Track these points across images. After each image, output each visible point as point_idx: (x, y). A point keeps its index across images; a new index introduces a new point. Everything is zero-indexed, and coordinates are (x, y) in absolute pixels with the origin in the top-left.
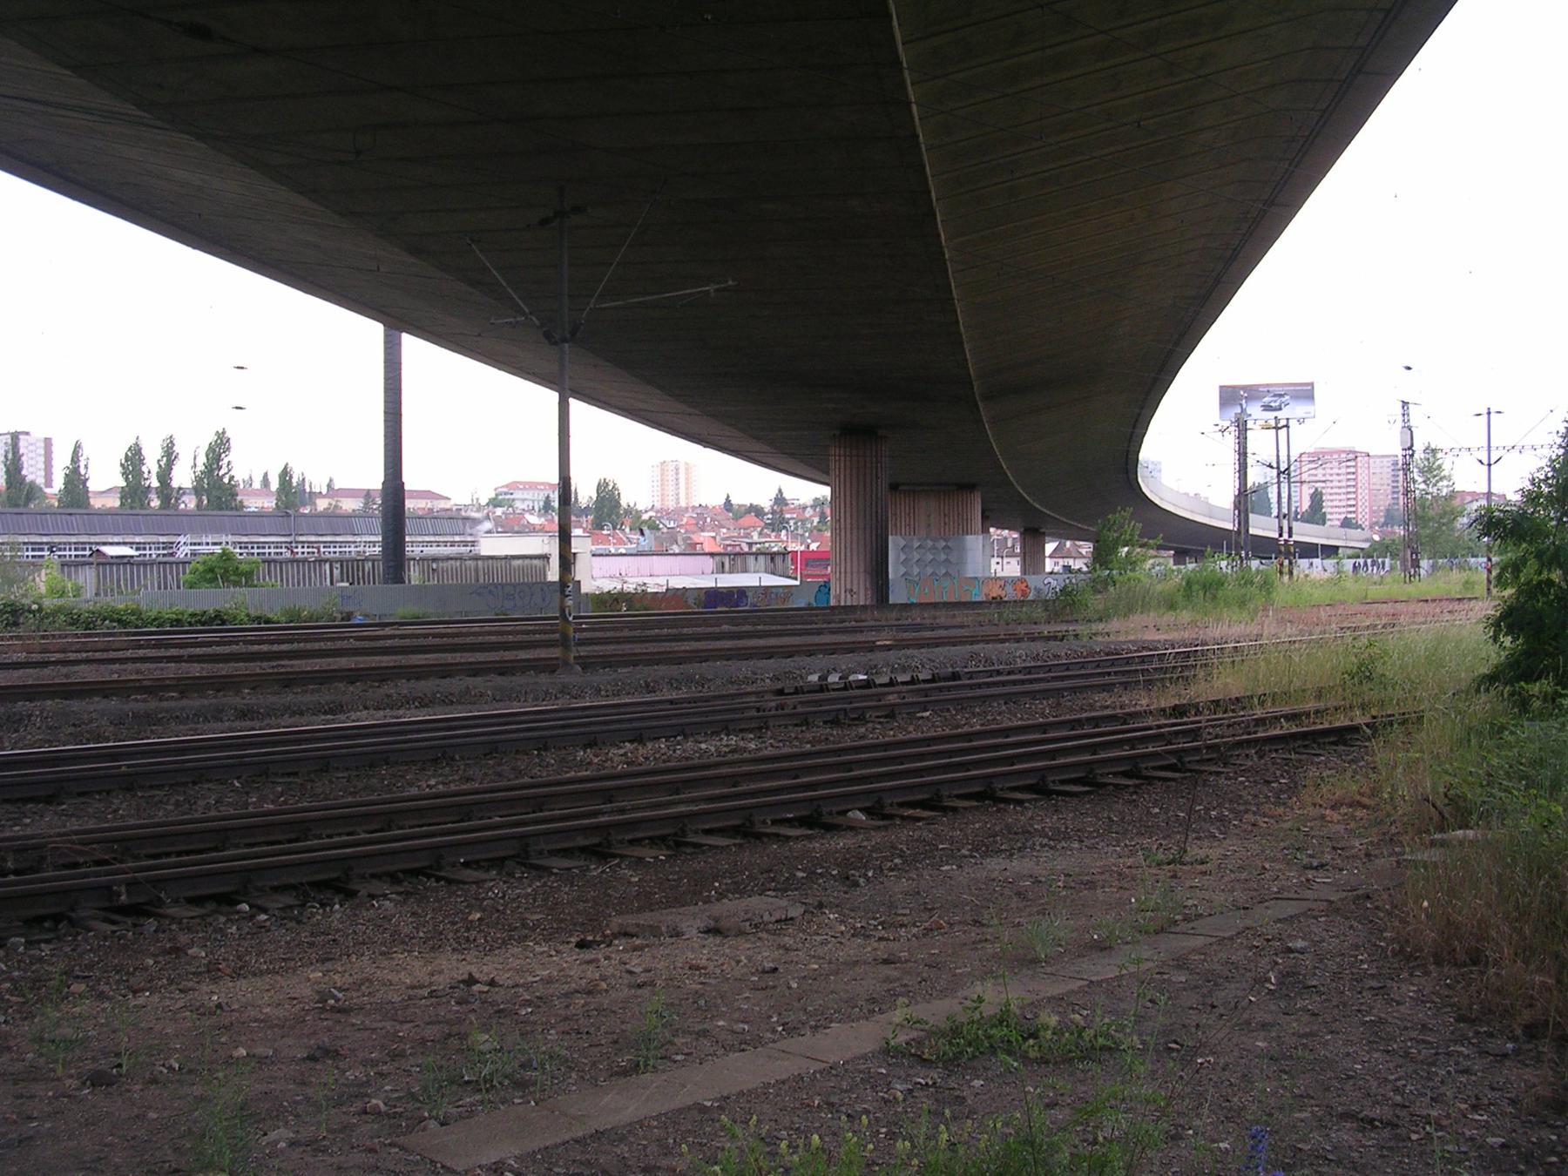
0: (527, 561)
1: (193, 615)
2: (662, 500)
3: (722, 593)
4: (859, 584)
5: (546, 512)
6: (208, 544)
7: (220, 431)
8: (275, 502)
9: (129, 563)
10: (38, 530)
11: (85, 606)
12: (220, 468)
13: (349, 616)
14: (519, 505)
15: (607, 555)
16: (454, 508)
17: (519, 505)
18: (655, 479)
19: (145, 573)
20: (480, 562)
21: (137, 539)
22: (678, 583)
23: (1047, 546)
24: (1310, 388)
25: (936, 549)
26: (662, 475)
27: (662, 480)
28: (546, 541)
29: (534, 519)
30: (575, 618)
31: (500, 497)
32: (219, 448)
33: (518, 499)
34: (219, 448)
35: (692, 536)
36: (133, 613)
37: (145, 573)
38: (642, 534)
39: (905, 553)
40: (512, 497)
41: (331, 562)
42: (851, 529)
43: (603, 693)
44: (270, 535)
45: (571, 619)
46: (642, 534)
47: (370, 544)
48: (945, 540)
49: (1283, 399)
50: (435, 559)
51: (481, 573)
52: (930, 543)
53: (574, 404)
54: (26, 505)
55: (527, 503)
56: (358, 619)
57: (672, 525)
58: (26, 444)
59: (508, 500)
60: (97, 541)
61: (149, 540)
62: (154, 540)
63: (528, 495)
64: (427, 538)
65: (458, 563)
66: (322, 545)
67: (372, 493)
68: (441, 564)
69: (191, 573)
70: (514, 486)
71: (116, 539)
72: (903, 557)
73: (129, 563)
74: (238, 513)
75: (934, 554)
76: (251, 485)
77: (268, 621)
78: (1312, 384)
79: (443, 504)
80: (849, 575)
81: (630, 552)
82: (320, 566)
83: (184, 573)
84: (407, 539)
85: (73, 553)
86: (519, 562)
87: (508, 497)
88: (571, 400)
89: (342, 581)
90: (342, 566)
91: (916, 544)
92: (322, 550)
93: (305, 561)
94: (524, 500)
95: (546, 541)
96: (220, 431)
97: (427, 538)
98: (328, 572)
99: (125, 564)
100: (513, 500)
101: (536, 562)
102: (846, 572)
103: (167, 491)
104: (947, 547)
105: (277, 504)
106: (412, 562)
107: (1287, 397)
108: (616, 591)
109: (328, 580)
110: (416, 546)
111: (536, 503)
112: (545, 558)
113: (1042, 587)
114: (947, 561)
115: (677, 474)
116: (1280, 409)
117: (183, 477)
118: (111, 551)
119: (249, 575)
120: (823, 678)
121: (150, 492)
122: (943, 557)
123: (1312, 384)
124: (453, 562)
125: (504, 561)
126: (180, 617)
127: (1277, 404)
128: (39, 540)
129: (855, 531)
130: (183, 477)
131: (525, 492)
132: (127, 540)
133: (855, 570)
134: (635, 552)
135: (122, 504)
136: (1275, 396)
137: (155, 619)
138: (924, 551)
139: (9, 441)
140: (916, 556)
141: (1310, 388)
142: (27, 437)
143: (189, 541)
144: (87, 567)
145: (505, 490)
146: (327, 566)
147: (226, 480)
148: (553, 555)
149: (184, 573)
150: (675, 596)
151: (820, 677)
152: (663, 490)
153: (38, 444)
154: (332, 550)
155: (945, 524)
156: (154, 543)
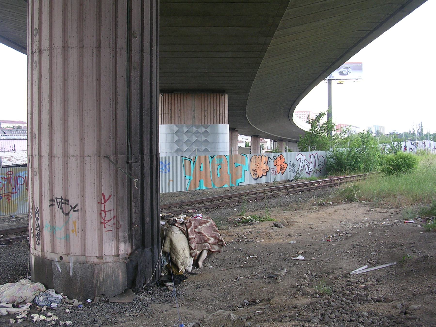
4: (210, 111)
24: (360, 65)
25: (199, 133)
39: (178, 136)
42: (65, 48)
48: (205, 127)
49: (349, 70)
52: (194, 129)
72: (176, 138)
75: (206, 137)
78: (361, 64)
80: (58, 163)
91: (185, 130)
102: (51, 156)
104: (206, 132)
107: (350, 69)
113: (295, 162)
114: (206, 141)
116: (347, 74)
122: (203, 138)
123: (361, 64)
127: (346, 72)
129: (73, 54)
133: (73, 150)
136: (345, 68)
138: (190, 134)
140: (185, 138)
141: (360, 65)
155: (205, 116)
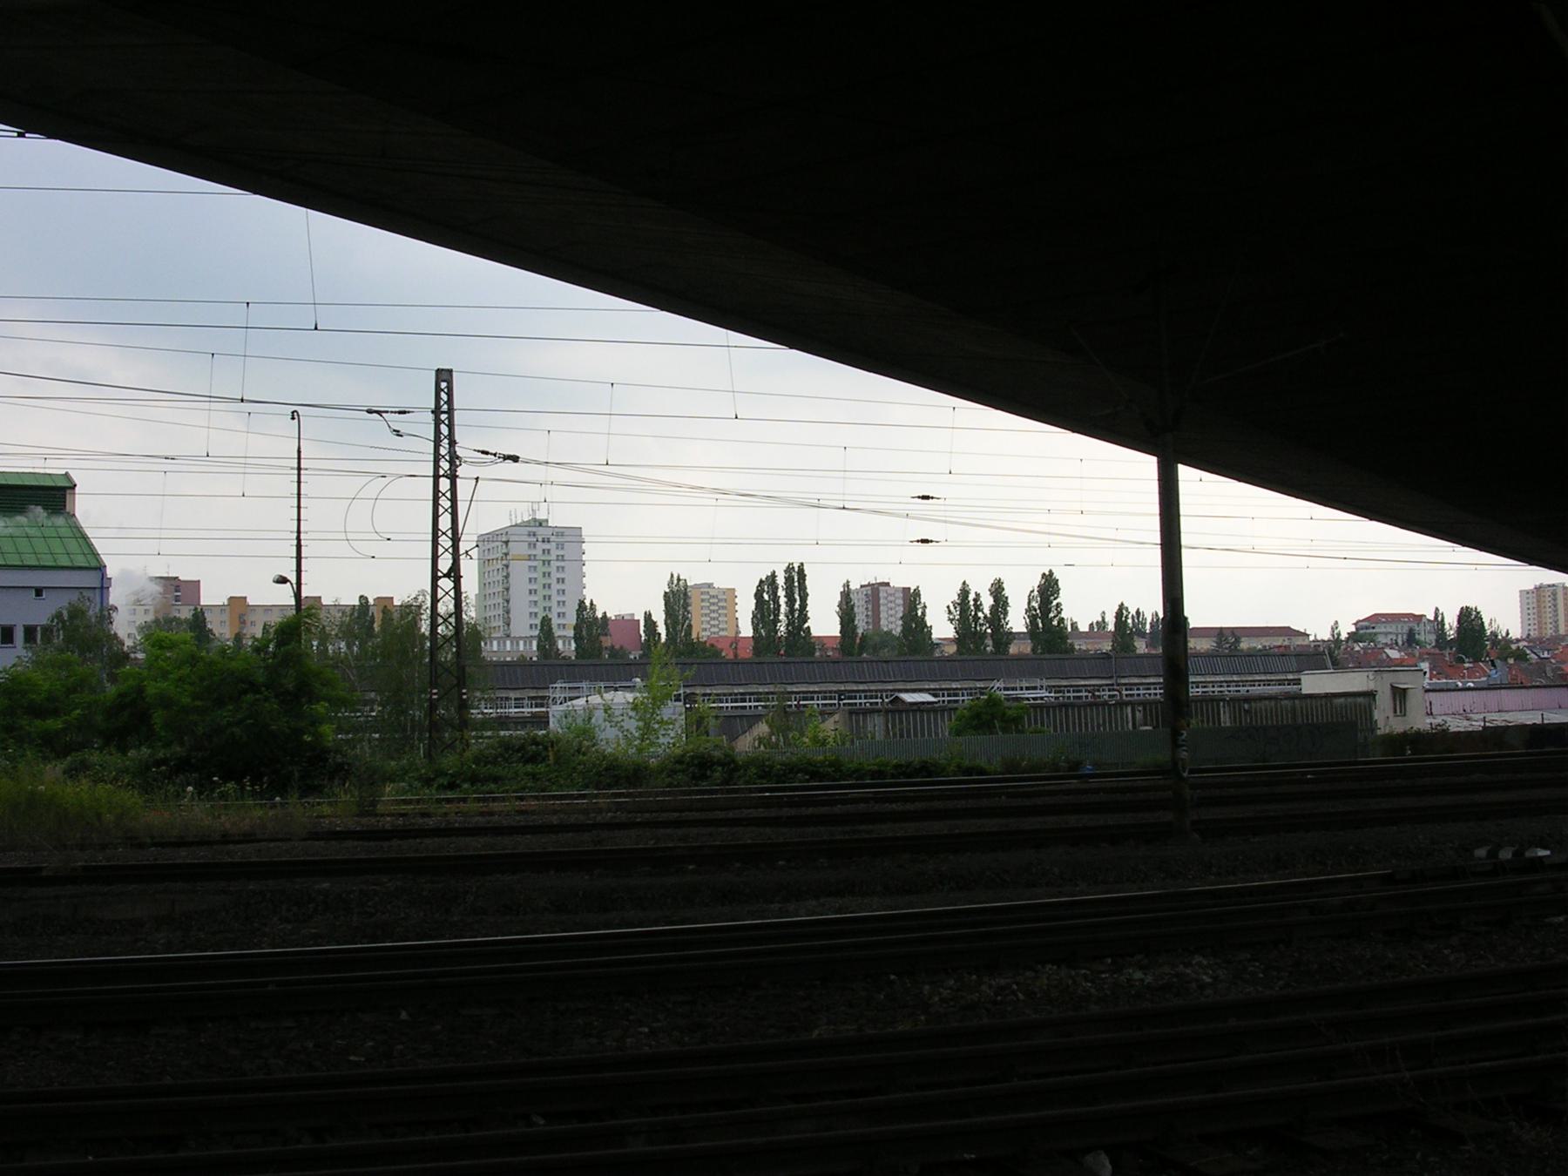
0: (1350, 700)
1: (897, 766)
2: (1540, 628)
3: (1423, 735)
5: (1410, 645)
6: (1021, 689)
7: (1047, 573)
8: (1111, 644)
9: (919, 710)
10: (854, 677)
11: (779, 758)
12: (1050, 611)
13: (1076, 765)
14: (1382, 639)
15: (1454, 690)
16: (1312, 645)
17: (1382, 639)
18: (1531, 606)
19: (935, 719)
20: (1297, 702)
21: (932, 686)
22: (1498, 719)
23: (1161, 651)
26: (1538, 601)
27: (1539, 606)
28: (1371, 677)
29: (1394, 654)
30: (1191, 771)
31: (1361, 632)
32: (1049, 587)
33: (1380, 633)
34: (1049, 587)
35: (1563, 666)
36: (831, 764)
37: (935, 719)
38: (1493, 665)
40: (1374, 631)
41: (1133, 704)
43: (1214, 870)
44: (1091, 678)
45: (1185, 775)
46: (1493, 665)
47: (1152, 688)
50: (1247, 700)
51: (1349, 709)
53: (1186, 473)
54: (860, 654)
55: (1390, 637)
56: (1088, 768)
57: (1546, 655)
58: (885, 595)
59: (1370, 634)
60: (913, 687)
61: (725, 691)
62: (972, 686)
63: (1391, 628)
64: (1257, 678)
65: (1273, 703)
66: (1124, 688)
67: (1224, 632)
68: (1253, 704)
69: (956, 720)
70: (1376, 619)
71: (913, 686)
73: (919, 710)
74: (1067, 656)
76: (1104, 628)
77: (982, 772)
79: (1299, 641)
81: (1479, 686)
82: (1121, 710)
83: (950, 720)
84: (1192, 679)
85: (946, 699)
86: (1342, 700)
87: (1371, 631)
88: (1186, 473)
89: (1146, 725)
90: (1145, 709)
92: (1124, 692)
93: (1105, 704)
94: (1386, 634)
95: (1371, 677)
96: (1047, 573)
97: (1257, 678)
98: (1130, 715)
99: (914, 711)
100: (1375, 634)
101: (1360, 700)
103: (1003, 638)
105: (1113, 646)
106: (1222, 704)
108: (1413, 731)
109: (1130, 724)
110: (1199, 685)
111: (1400, 636)
112: (1371, 695)
115: (1555, 600)
117: (1017, 621)
118: (909, 698)
119: (1017, 720)
120: (1493, 854)
121: (986, 637)
124: (1267, 702)
125: (1324, 699)
126: (882, 768)
128: (855, 688)
130: (1017, 621)
131: (1388, 625)
132: (943, 687)
134: (1486, 686)
135: (1033, 650)
137: (854, 772)
139: (869, 592)
142: (887, 588)
143: (1002, 686)
144: (876, 714)
145: (1366, 624)
146: (1129, 709)
147: (1055, 623)
148: (1380, 693)
149: (950, 720)
150: (1494, 736)
151: (1489, 852)
152: (1540, 617)
153: (897, 595)
154: (1153, 691)
156: (966, 689)
